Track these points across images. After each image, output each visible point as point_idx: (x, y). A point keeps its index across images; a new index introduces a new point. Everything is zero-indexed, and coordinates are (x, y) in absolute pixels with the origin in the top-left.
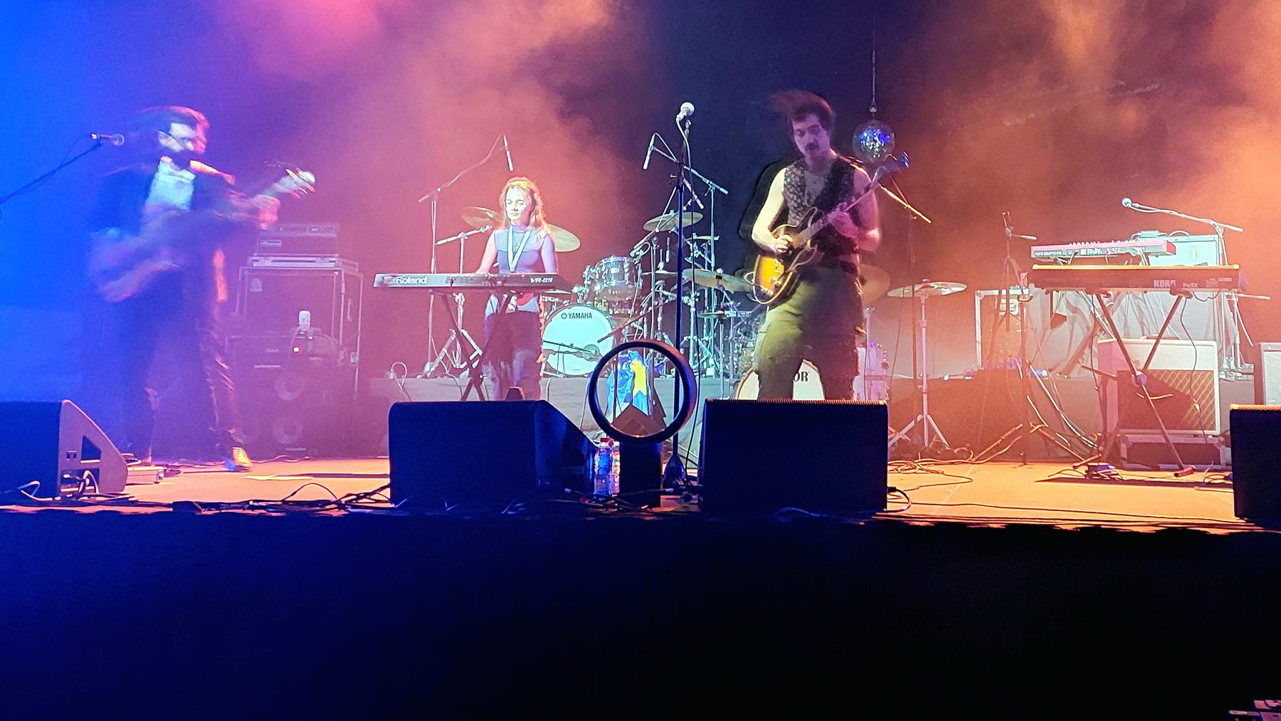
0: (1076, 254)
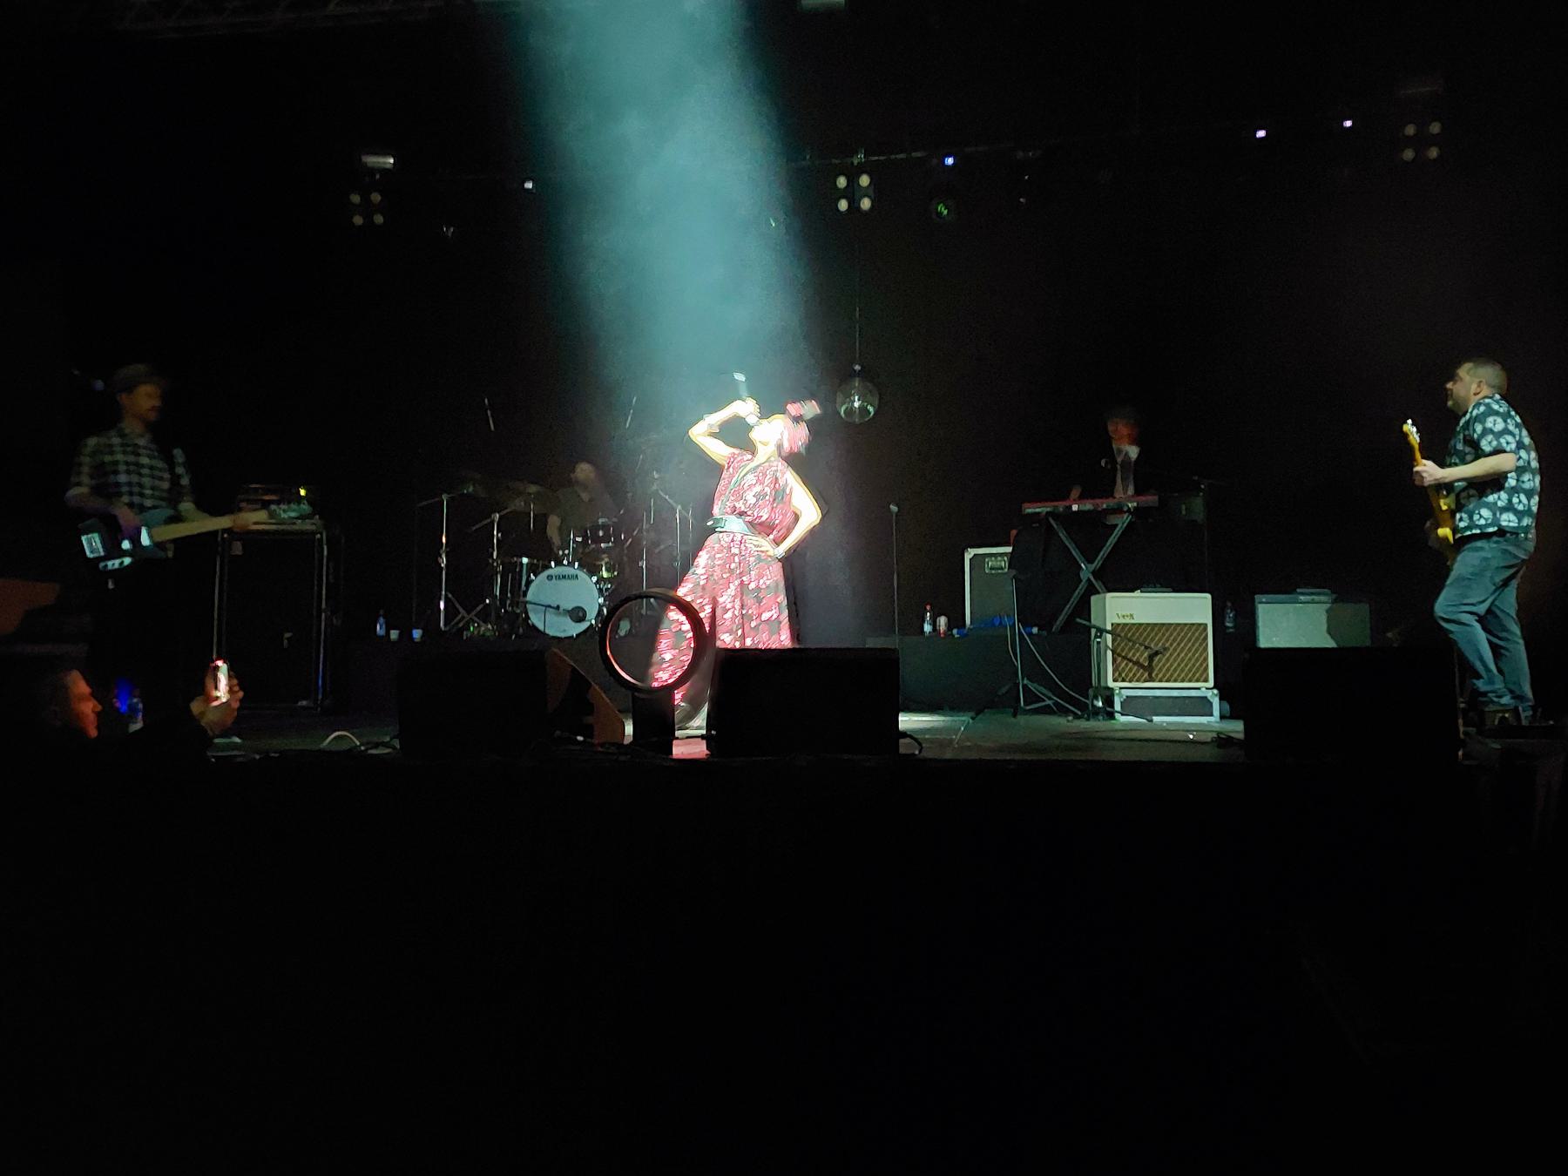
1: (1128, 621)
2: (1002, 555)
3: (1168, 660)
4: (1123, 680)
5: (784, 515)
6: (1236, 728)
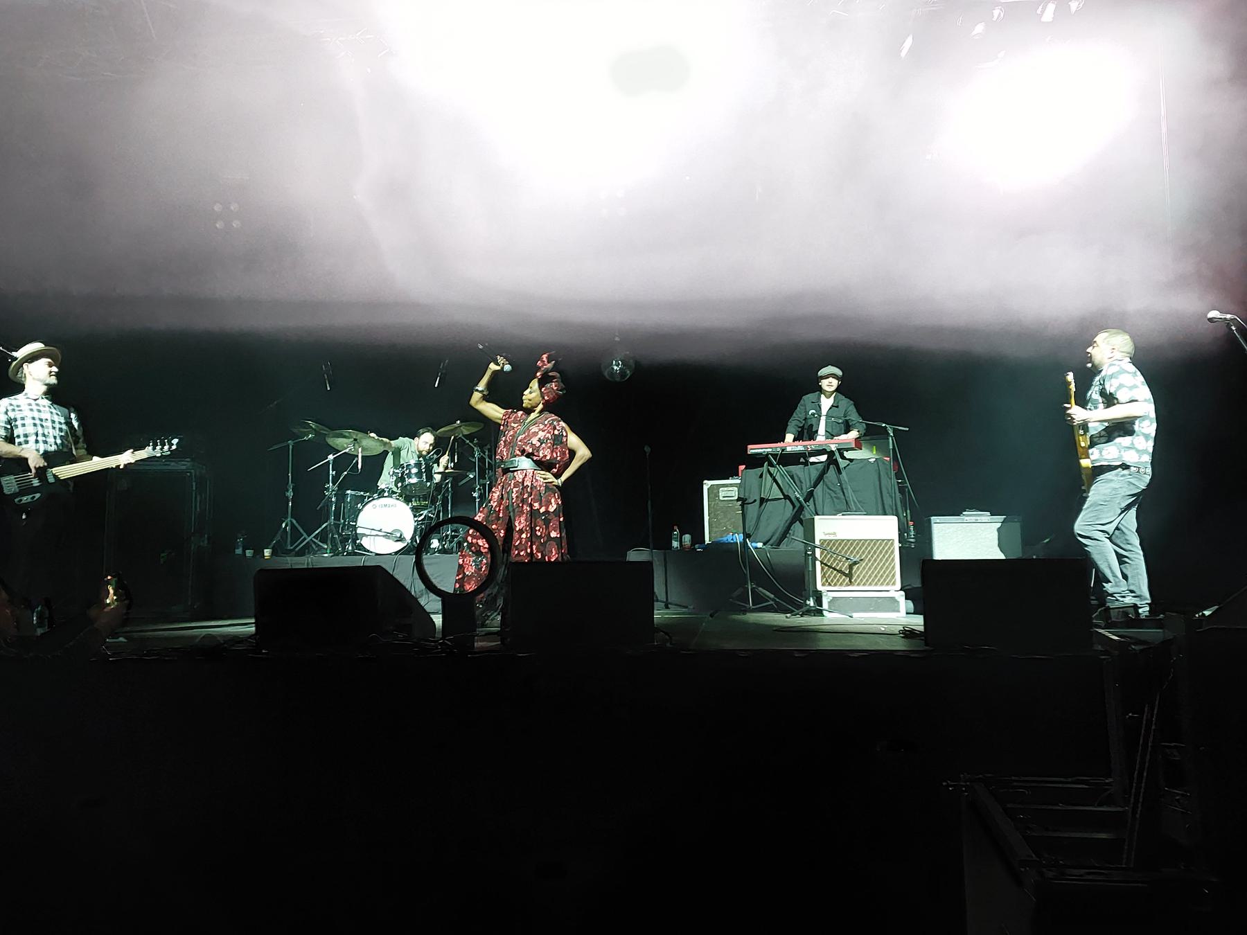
0: (783, 450)
1: (832, 537)
2: (731, 485)
3: (864, 568)
4: (830, 584)
5: (564, 453)
6: (918, 622)
